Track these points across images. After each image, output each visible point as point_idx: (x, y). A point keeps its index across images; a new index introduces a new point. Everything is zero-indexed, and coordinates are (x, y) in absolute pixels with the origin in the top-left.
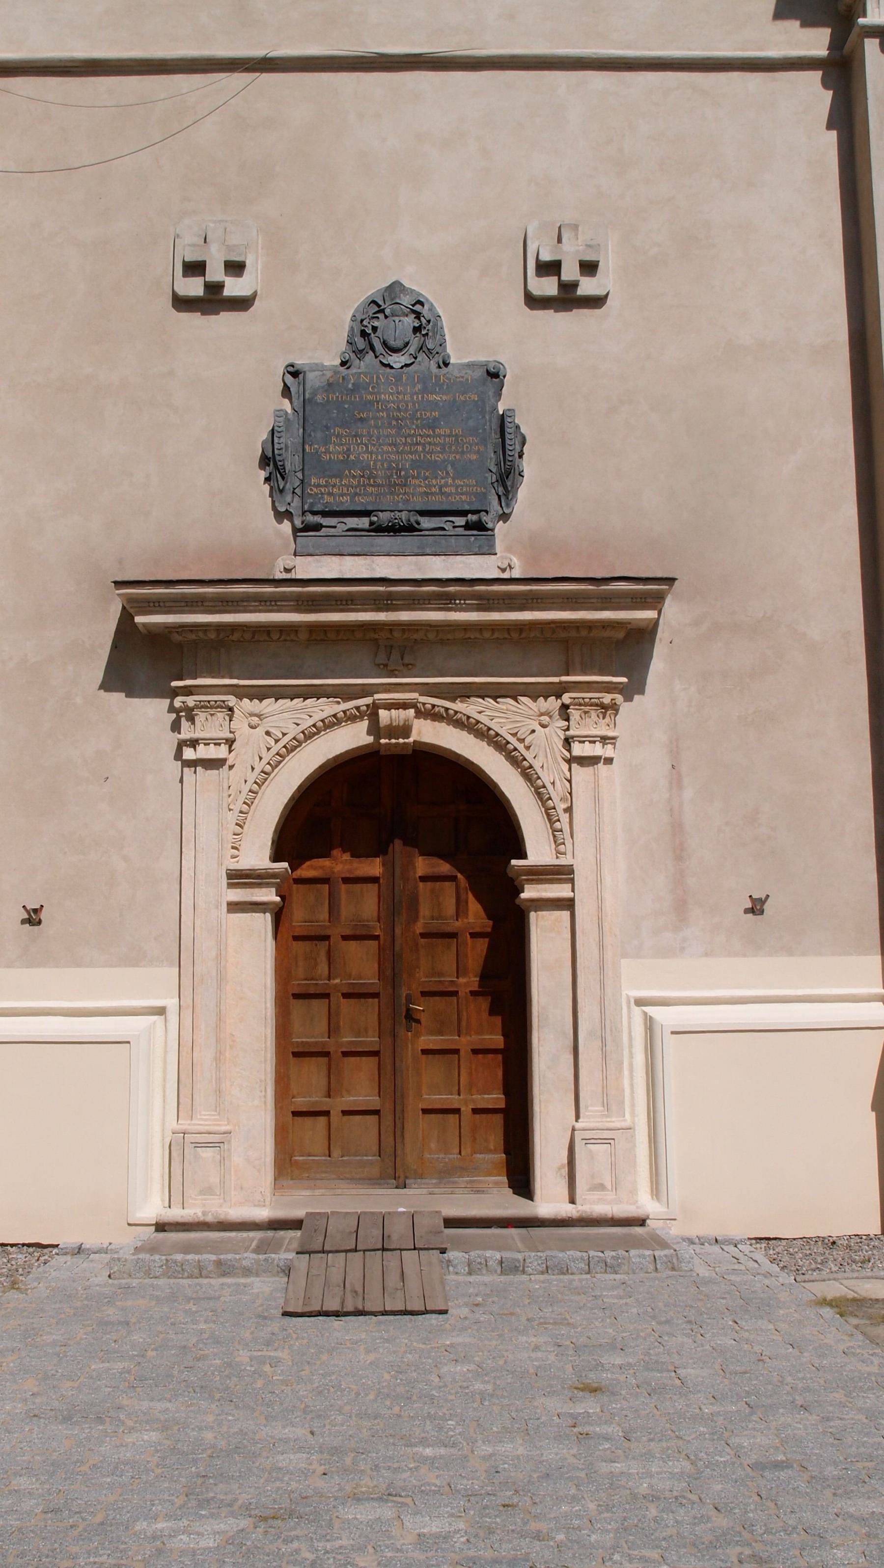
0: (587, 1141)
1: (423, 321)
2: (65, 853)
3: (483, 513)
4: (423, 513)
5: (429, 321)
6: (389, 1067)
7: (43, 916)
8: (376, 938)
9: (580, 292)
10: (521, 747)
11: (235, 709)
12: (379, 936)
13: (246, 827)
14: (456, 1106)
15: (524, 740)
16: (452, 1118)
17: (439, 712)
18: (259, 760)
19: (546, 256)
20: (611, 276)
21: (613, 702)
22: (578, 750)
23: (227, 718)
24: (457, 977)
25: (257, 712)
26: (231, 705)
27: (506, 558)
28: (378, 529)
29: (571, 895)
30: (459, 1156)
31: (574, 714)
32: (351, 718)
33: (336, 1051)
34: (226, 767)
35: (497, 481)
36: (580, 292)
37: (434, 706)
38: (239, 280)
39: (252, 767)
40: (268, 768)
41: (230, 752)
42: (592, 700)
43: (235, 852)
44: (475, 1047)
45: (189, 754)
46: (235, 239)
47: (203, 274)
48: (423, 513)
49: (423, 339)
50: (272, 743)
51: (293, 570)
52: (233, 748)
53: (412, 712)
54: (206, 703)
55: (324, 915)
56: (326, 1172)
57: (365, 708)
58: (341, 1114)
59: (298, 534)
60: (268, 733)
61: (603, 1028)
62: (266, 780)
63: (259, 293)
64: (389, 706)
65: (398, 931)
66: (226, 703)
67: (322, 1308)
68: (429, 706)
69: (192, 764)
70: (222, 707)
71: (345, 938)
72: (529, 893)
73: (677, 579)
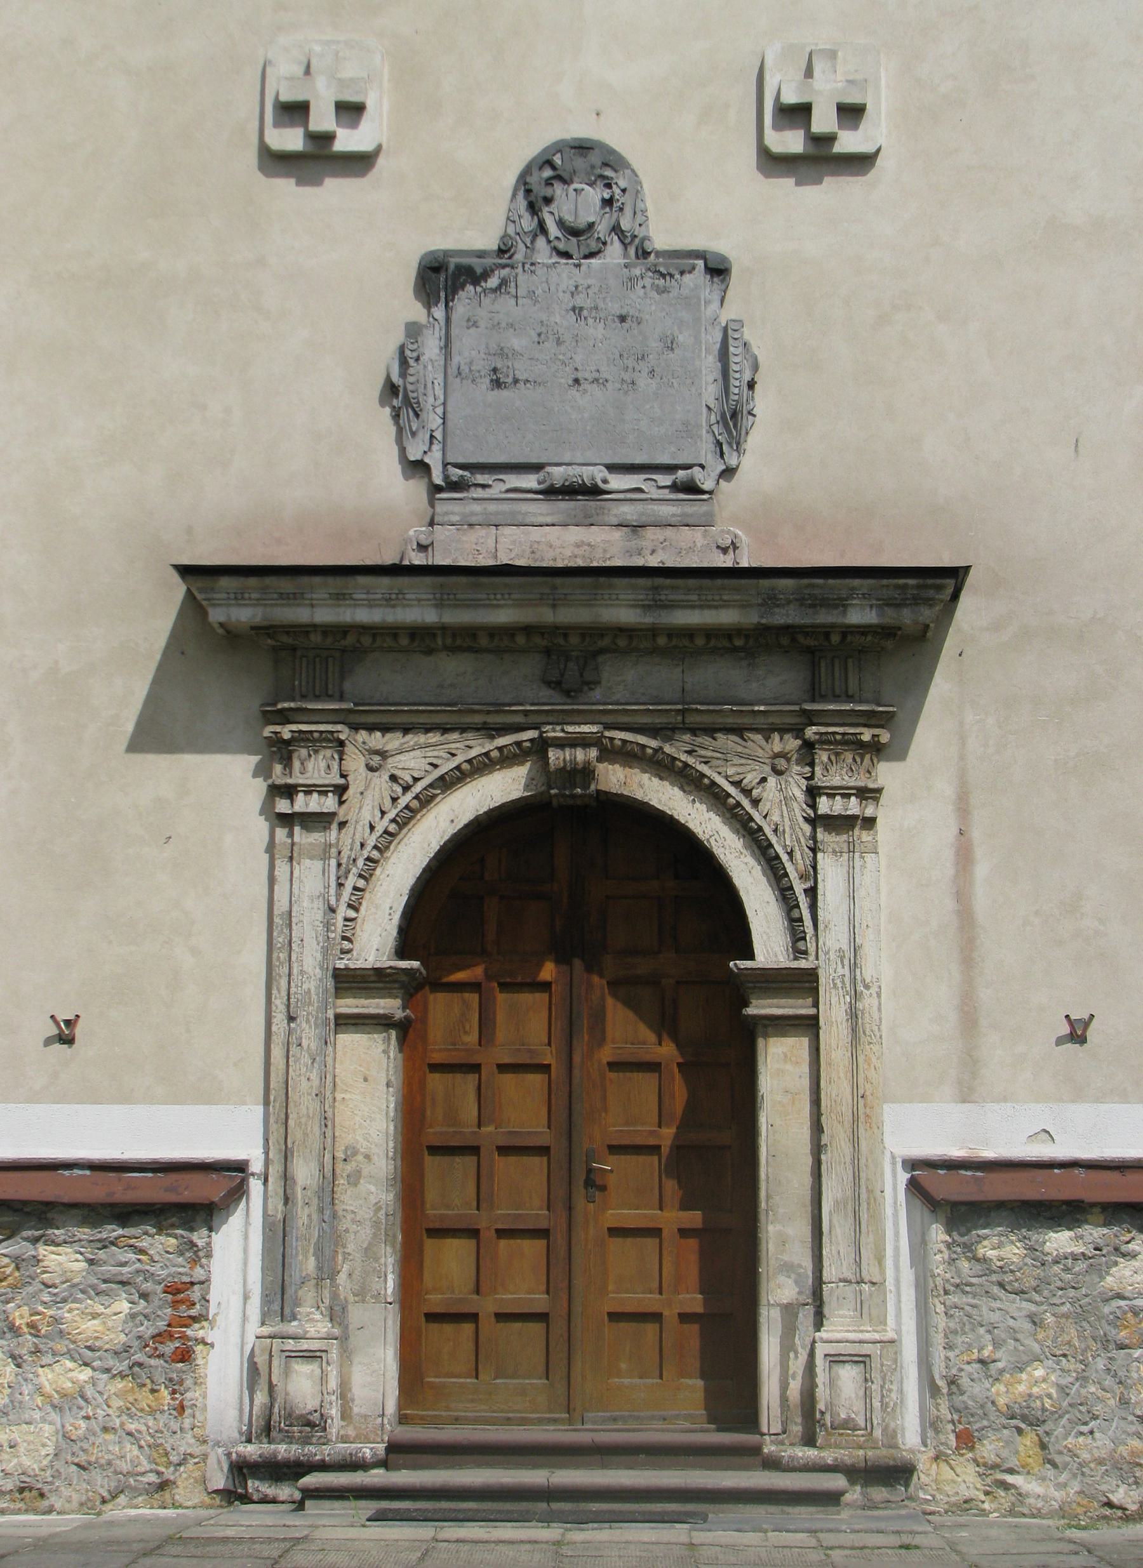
0: (835, 1360)
1: (617, 191)
2: (110, 942)
3: (696, 469)
4: (612, 468)
5: (624, 191)
6: (563, 1252)
7: (79, 1031)
8: (545, 1068)
9: (838, 148)
10: (746, 803)
11: (347, 742)
12: (549, 1066)
13: (363, 909)
14: (655, 1308)
15: (751, 791)
16: (651, 1329)
17: (632, 749)
18: (380, 815)
19: (790, 97)
20: (883, 123)
21: (876, 739)
22: (824, 805)
23: (336, 756)
24: (660, 1127)
25: (379, 747)
26: (342, 737)
27: (729, 532)
28: (551, 492)
29: (812, 1011)
30: (659, 1381)
31: (822, 756)
32: (506, 759)
33: (488, 1228)
34: (334, 826)
35: (718, 422)
36: (838, 148)
37: (624, 742)
38: (355, 132)
39: (371, 825)
40: (392, 828)
41: (341, 803)
42: (846, 737)
43: (346, 945)
44: (683, 1226)
45: (283, 806)
46: (349, 71)
47: (305, 122)
48: (612, 468)
49: (615, 215)
50: (399, 790)
51: (430, 549)
52: (344, 798)
53: (593, 753)
54: (309, 736)
55: (472, 1038)
56: (472, 1401)
57: (528, 744)
58: (493, 1319)
59: (438, 496)
60: (393, 778)
61: (857, 1198)
62: (390, 843)
63: (384, 146)
64: (561, 744)
65: (577, 1059)
66: (335, 735)
67: (402, 559)
68: (619, 743)
69: (287, 820)
70: (330, 741)
71: (503, 1068)
72: (759, 1007)
73: (970, 567)
